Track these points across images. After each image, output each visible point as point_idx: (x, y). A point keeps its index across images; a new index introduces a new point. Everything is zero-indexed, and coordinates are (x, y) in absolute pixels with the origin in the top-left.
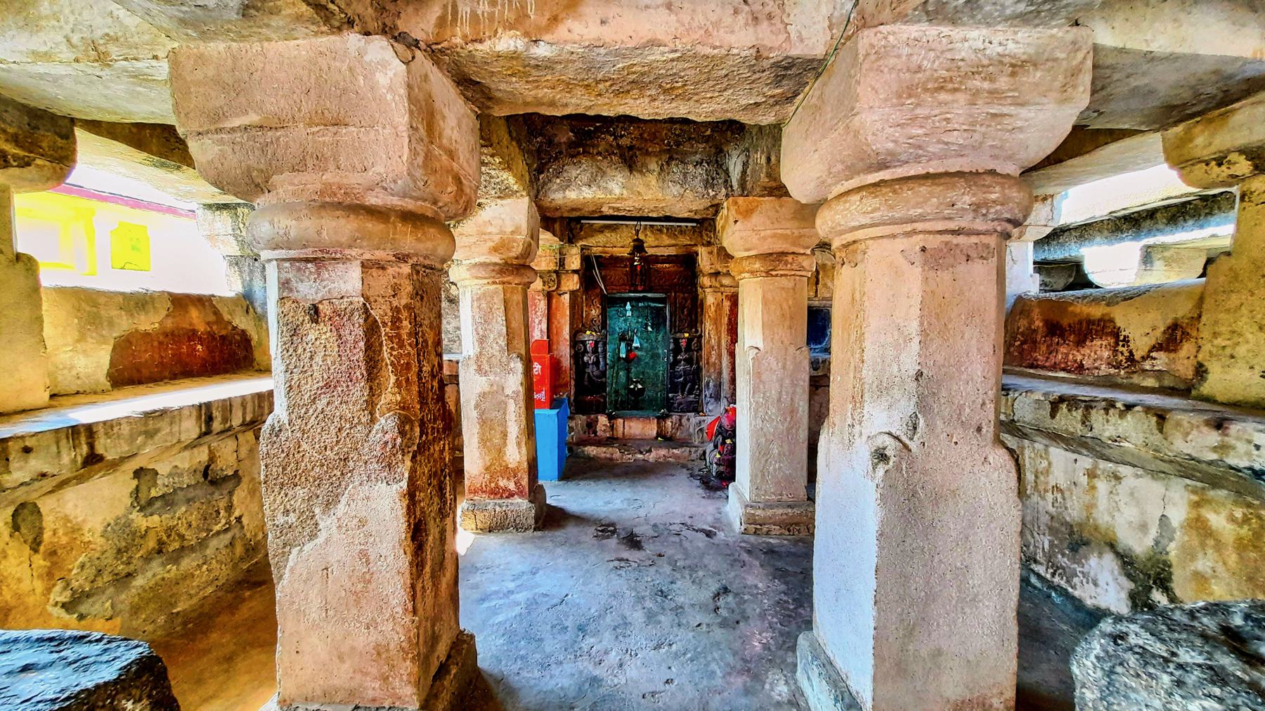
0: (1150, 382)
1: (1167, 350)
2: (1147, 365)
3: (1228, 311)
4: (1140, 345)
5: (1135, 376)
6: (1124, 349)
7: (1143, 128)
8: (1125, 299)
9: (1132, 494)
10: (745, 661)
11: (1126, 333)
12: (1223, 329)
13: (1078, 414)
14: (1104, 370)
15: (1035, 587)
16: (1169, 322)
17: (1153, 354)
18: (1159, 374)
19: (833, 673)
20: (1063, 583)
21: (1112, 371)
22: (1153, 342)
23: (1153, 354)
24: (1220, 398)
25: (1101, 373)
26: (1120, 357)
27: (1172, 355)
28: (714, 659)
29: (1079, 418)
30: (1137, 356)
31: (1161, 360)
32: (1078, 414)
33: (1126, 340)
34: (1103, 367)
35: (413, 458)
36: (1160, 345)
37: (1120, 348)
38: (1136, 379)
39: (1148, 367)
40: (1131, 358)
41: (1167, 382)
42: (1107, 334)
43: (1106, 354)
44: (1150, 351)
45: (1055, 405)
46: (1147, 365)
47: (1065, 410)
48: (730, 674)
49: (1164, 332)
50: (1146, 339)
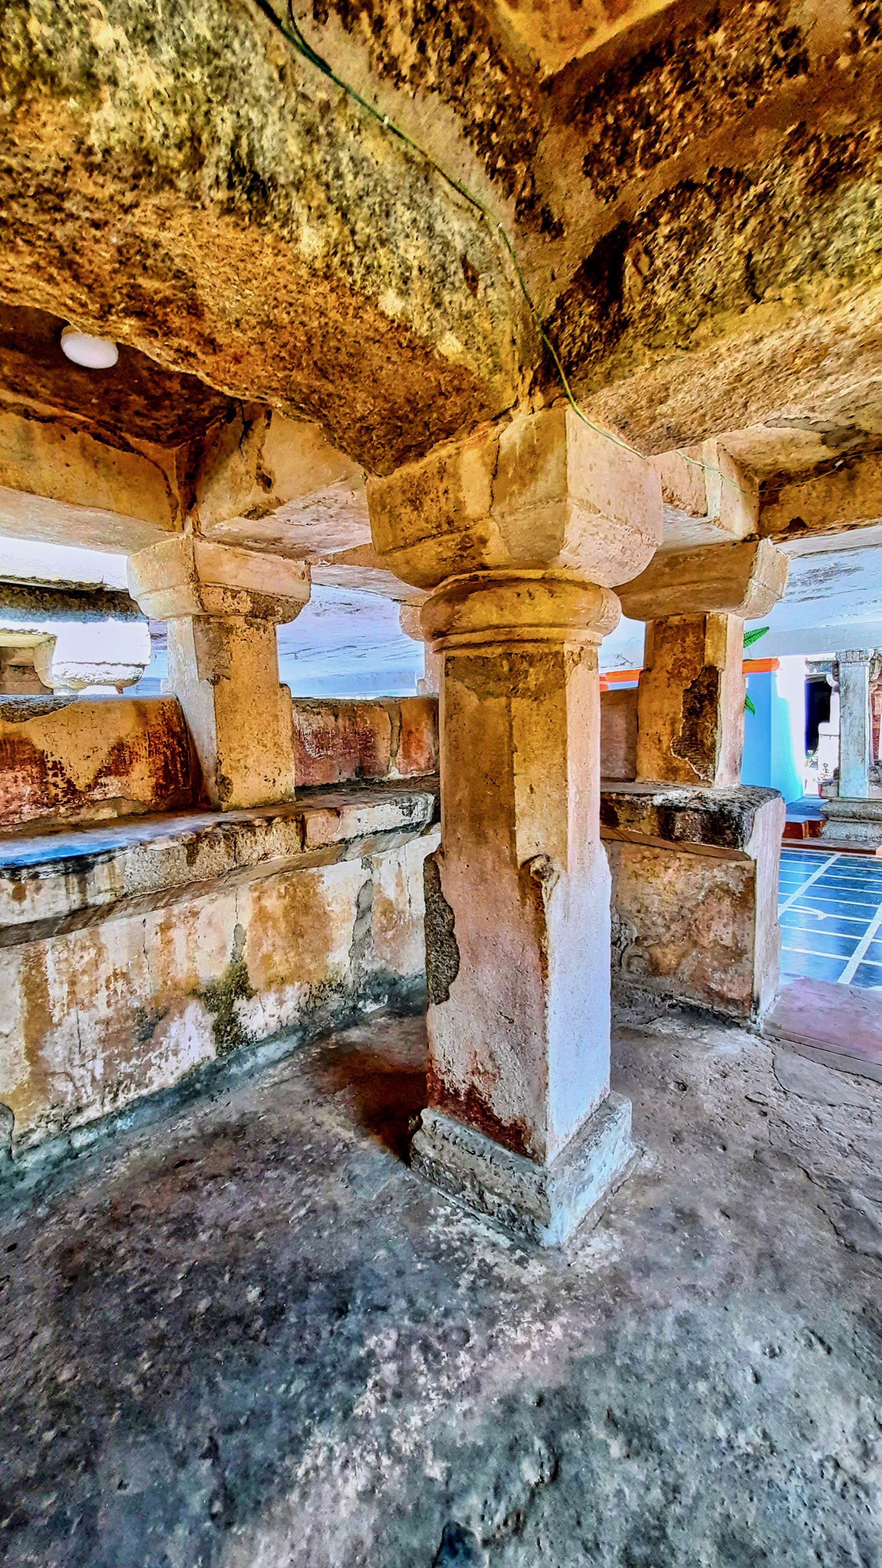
0: (106, 813)
1: (118, 773)
2: (97, 794)
3: (236, 728)
4: (82, 772)
5: (83, 810)
6: (58, 780)
7: (83, 502)
8: (36, 714)
9: (210, 923)
10: (608, 1313)
11: (56, 758)
12: (235, 745)
13: (221, 848)
14: (29, 813)
15: (90, 1145)
16: (113, 742)
17: (103, 780)
18: (115, 802)
19: (588, 1130)
20: (133, 1095)
21: (45, 811)
22: (97, 765)
23: (103, 780)
24: (244, 805)
25: (26, 818)
26: (53, 791)
27: (124, 779)
28: (659, 1346)
29: (223, 851)
30: (80, 785)
31: (113, 786)
32: (221, 848)
33: (58, 768)
34: (26, 809)
35: (60, 248)
36: (108, 769)
37: (51, 779)
38: (85, 814)
39: (98, 797)
40: (71, 789)
41: (126, 809)
42: (23, 762)
43: (27, 790)
44: (96, 778)
45: (192, 849)
46: (97, 794)
47: (207, 849)
48: (654, 1306)
49: (110, 754)
50: (88, 763)
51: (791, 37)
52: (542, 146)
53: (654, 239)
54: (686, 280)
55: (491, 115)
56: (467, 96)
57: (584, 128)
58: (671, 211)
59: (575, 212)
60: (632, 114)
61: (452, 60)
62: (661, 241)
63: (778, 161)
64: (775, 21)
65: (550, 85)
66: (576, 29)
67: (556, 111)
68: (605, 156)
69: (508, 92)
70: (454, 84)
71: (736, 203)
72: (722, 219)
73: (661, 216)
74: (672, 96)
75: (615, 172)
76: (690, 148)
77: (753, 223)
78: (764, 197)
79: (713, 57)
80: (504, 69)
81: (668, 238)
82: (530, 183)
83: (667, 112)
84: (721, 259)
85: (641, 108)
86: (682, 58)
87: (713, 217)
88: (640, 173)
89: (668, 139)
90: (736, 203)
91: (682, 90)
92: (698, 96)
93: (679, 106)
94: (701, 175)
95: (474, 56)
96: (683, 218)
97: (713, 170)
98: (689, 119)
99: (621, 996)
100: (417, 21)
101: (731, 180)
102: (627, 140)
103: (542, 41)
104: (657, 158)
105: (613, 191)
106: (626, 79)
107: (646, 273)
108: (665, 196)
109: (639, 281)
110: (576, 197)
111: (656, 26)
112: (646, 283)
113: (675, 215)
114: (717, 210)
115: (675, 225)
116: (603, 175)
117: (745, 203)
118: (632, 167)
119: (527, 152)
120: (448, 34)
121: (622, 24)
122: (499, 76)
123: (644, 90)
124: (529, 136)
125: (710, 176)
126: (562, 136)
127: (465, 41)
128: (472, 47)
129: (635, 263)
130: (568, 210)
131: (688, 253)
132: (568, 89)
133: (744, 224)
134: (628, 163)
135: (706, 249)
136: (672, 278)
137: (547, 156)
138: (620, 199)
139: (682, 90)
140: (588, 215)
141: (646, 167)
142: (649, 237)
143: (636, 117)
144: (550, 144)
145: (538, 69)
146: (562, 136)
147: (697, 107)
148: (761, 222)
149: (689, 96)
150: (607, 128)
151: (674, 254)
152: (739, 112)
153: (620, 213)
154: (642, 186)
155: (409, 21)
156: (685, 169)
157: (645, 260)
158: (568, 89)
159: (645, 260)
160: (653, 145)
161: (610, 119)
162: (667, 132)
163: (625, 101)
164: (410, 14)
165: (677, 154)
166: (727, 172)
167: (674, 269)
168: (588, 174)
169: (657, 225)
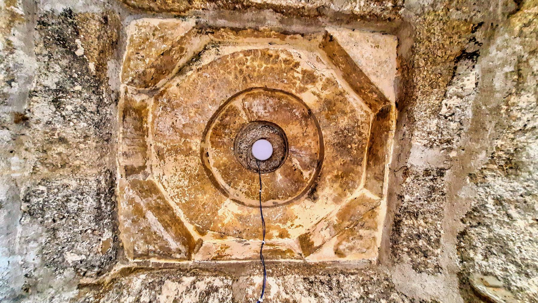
51: (427, 173)
52: (394, 281)
53: (480, 266)
54: (527, 266)
55: (362, 291)
56: (346, 294)
57: (400, 260)
58: (470, 248)
59: (433, 290)
60: (410, 240)
61: (331, 289)
62: (484, 263)
63: (481, 190)
64: (417, 177)
65: (379, 262)
66: (369, 242)
67: (387, 266)
68: (419, 260)
69: (361, 278)
70: (338, 295)
71: (491, 216)
72: (496, 228)
73: (469, 254)
74: (415, 223)
75: (429, 261)
76: (448, 224)
77: (513, 212)
78: (499, 201)
79: (413, 202)
80: (352, 274)
81: (486, 258)
82: (404, 297)
83: (420, 227)
84: (527, 238)
85: (411, 236)
86: (404, 213)
87: (490, 231)
88: (438, 251)
89: (432, 233)
90: (491, 216)
91: (416, 218)
92: (423, 213)
93: (422, 222)
94: (461, 227)
95: (338, 281)
96: (479, 245)
97: (462, 220)
98: (430, 220)
99: (210, 63)
100: (309, 290)
101: (475, 215)
102: (420, 248)
103: (363, 255)
104: (438, 241)
105: (438, 267)
106: (397, 236)
107: (501, 283)
108: (459, 247)
109: (503, 291)
110: (426, 284)
111: (389, 218)
112: (510, 289)
113: (474, 248)
114: (488, 226)
115: (480, 250)
116: (426, 266)
117: (495, 212)
118: (433, 253)
119: (391, 288)
120: (322, 283)
121: (381, 228)
122: (353, 277)
123: (405, 231)
124: (386, 283)
125: (464, 223)
126: (397, 271)
127: (329, 281)
128: (335, 279)
129: (488, 286)
130: (429, 292)
131: (506, 254)
132: (385, 257)
133: (509, 216)
134: (429, 253)
135: (511, 244)
136: (519, 273)
137: (399, 282)
138: (444, 266)
139: (416, 218)
140: (441, 286)
141: (438, 247)
142: (477, 268)
143: (413, 240)
144: (396, 279)
145: (371, 262)
146: (397, 271)
147: (428, 215)
148: (516, 207)
149: (420, 216)
150: (408, 253)
151: (500, 261)
152: (443, 200)
153: (452, 272)
154: (447, 255)
155: (306, 293)
156: (452, 232)
157: (490, 280)
158: (385, 257)
159: (490, 280)
160: (430, 240)
161: (406, 249)
162: (429, 231)
163: (404, 240)
164: (304, 290)
165: (442, 232)
166: (468, 214)
167: (512, 267)
168: (420, 272)
169: (472, 260)
